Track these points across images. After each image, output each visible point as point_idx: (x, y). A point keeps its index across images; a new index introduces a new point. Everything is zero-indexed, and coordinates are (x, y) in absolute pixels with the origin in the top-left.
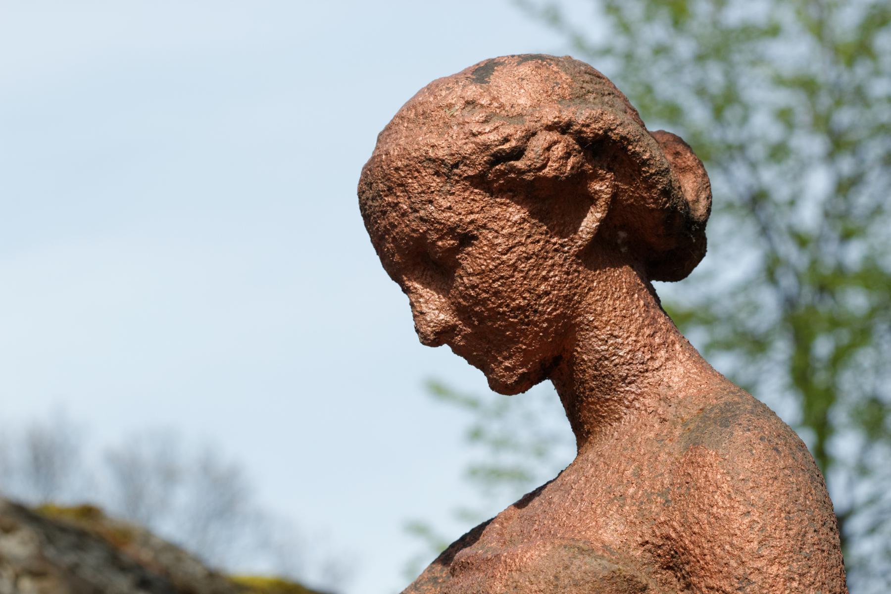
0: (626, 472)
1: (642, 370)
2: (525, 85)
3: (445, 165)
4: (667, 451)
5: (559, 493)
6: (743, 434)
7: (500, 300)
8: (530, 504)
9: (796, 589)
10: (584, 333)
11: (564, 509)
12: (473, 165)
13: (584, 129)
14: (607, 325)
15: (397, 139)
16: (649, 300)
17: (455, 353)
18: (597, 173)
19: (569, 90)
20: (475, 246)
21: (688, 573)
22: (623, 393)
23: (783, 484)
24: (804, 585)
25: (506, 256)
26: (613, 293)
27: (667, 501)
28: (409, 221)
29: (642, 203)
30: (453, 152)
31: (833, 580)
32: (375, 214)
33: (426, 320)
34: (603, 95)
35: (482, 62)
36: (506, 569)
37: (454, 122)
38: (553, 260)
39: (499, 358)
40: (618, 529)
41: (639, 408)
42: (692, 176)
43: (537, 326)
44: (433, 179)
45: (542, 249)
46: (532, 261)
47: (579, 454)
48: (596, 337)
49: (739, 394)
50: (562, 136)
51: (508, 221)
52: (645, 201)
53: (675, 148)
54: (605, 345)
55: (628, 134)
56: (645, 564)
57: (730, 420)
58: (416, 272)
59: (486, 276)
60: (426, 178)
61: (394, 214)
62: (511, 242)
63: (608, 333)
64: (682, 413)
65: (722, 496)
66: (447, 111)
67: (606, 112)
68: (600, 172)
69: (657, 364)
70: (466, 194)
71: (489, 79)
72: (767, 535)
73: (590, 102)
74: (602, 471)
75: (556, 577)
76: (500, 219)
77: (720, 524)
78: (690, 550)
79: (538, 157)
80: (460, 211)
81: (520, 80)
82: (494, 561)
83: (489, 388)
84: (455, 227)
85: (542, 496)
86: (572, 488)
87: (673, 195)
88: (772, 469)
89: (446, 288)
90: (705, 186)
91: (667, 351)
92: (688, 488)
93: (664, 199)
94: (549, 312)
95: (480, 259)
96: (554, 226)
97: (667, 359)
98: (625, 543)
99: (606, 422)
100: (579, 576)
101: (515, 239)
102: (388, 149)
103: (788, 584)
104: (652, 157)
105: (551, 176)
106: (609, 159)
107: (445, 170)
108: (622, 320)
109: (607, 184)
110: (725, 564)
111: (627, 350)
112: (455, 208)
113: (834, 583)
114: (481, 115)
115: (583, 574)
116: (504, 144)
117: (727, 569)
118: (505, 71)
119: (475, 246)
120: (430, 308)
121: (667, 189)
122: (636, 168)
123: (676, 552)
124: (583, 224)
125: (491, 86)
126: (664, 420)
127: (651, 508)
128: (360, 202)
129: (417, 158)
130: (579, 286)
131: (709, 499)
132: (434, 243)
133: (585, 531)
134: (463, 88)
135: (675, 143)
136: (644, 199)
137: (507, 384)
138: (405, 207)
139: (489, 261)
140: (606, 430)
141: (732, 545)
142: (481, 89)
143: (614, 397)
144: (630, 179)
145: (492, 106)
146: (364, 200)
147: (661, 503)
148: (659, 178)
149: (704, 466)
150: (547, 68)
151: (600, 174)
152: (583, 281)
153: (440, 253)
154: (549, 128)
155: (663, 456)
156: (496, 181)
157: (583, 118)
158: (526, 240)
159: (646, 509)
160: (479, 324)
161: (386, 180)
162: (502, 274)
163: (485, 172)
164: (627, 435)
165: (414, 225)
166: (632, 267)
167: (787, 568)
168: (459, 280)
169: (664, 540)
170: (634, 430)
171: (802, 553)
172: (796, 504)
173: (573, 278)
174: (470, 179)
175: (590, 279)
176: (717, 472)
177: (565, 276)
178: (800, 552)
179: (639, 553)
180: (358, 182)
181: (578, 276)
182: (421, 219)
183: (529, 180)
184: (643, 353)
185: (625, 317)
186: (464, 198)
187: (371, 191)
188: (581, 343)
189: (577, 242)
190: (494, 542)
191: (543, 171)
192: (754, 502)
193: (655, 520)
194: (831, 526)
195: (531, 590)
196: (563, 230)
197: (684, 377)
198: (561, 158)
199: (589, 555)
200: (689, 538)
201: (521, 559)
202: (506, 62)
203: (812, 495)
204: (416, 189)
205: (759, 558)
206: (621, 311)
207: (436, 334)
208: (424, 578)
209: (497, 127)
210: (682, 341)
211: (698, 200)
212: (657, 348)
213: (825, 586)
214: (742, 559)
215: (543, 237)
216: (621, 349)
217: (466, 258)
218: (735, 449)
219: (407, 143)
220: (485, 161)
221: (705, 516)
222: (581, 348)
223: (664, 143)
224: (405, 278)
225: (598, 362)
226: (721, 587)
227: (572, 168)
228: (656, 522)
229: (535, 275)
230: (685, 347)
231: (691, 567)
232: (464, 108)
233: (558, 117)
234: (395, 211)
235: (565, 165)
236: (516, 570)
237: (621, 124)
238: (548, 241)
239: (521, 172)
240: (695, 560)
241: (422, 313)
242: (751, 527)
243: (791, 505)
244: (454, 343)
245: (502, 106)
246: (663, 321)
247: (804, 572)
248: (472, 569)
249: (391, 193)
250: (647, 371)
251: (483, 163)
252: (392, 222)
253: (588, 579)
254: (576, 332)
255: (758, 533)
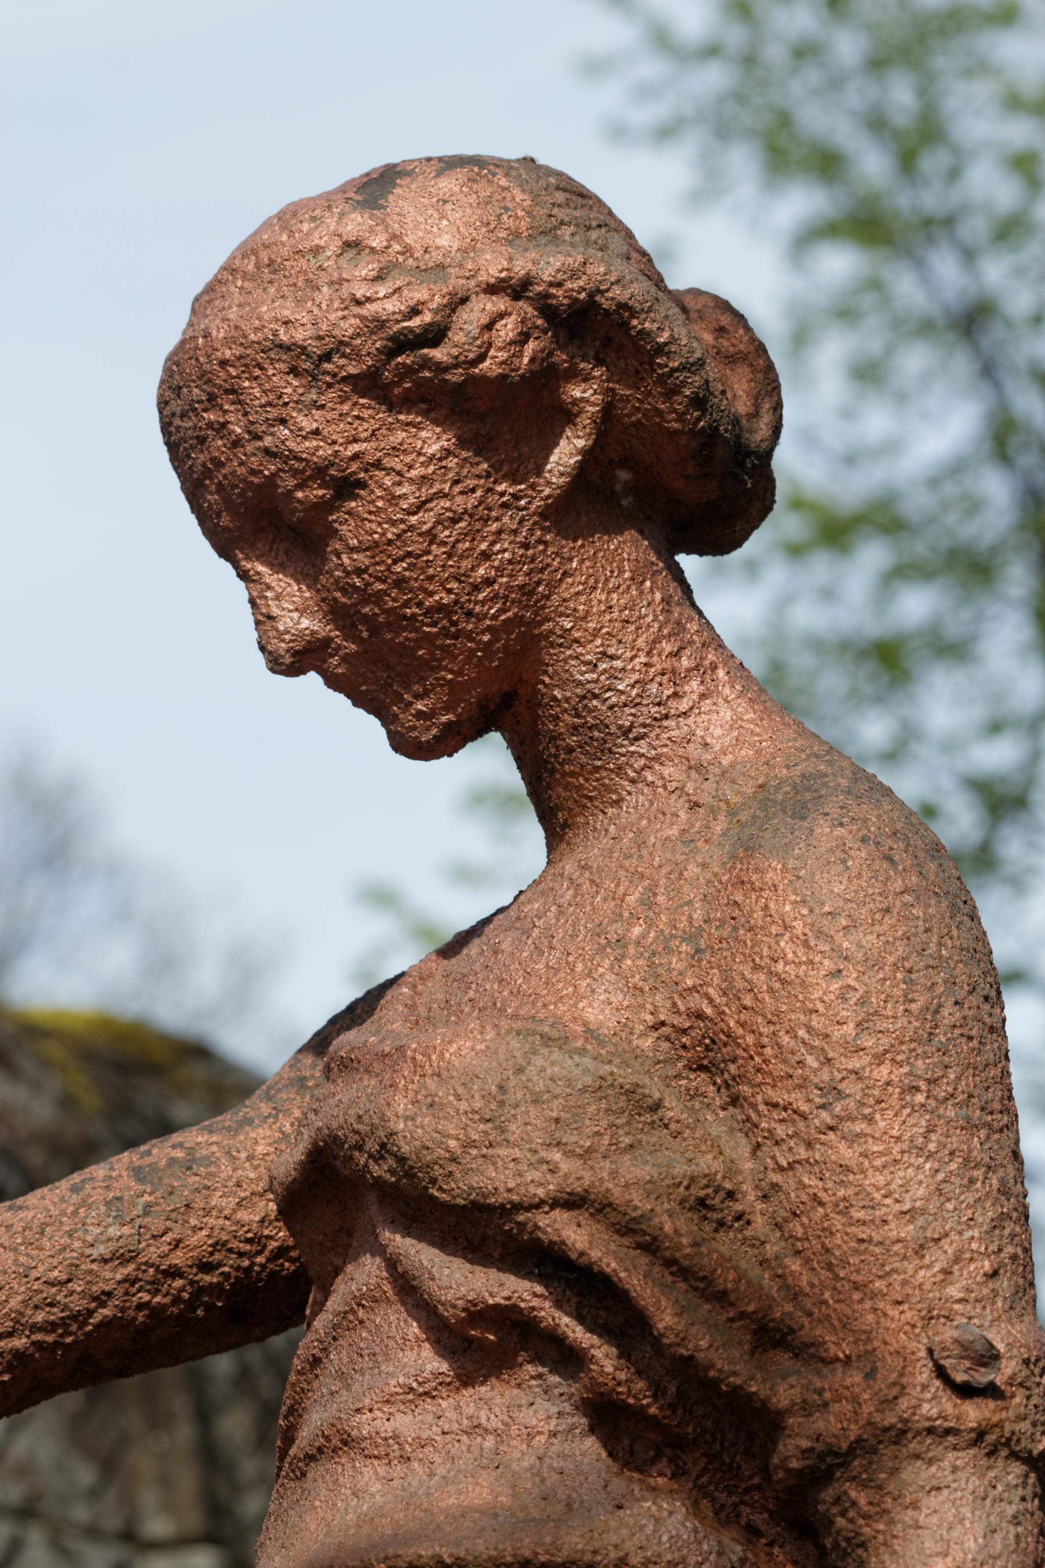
0: (628, 898)
1: (658, 715)
2: (449, 212)
3: (308, 355)
4: (700, 860)
5: (512, 934)
6: (832, 831)
7: (406, 594)
8: (465, 951)
9: (923, 1106)
10: (556, 651)
11: (520, 964)
12: (356, 355)
13: (553, 291)
14: (595, 636)
15: (224, 308)
16: (671, 591)
17: (329, 687)
18: (576, 368)
19: (528, 219)
20: (362, 498)
21: (734, 1079)
22: (624, 756)
23: (899, 921)
24: (936, 1099)
25: (416, 517)
26: (607, 580)
27: (698, 951)
28: (245, 455)
29: (657, 420)
30: (321, 333)
31: (987, 1088)
32: (186, 442)
33: (277, 630)
34: (589, 228)
35: (375, 170)
36: (415, 1072)
37: (323, 279)
38: (499, 524)
39: (406, 696)
40: (613, 999)
41: (653, 783)
42: (747, 370)
43: (472, 640)
44: (287, 381)
45: (480, 504)
46: (463, 524)
47: (549, 862)
48: (577, 658)
49: (828, 758)
50: (513, 302)
51: (419, 454)
52: (662, 417)
53: (718, 320)
54: (593, 671)
55: (630, 299)
56: (659, 1062)
57: (810, 805)
58: (260, 545)
59: (381, 552)
60: (275, 379)
61: (220, 443)
62: (424, 493)
63: (598, 650)
64: (728, 792)
65: (793, 942)
66: (311, 259)
67: (591, 260)
68: (582, 365)
69: (684, 705)
70: (346, 408)
71: (387, 201)
72: (871, 1011)
73: (564, 241)
74: (587, 896)
75: (501, 1088)
76: (405, 450)
77: (789, 992)
78: (737, 1038)
79: (471, 341)
80: (333, 437)
81: (441, 203)
82: (395, 1057)
83: (390, 748)
84: (327, 466)
85: (484, 938)
86: (535, 926)
87: (711, 407)
88: (880, 894)
89: (311, 572)
90: (769, 389)
91: (702, 682)
92: (735, 929)
93: (695, 414)
94: (493, 615)
95: (371, 521)
96: (501, 463)
97: (703, 696)
98: (625, 1025)
99: (596, 807)
100: (541, 1084)
101: (431, 487)
102: (207, 328)
103: (908, 1098)
104: (673, 341)
105: (495, 374)
106: (598, 343)
107: (307, 365)
108: (623, 627)
109: (595, 387)
110: (798, 1063)
111: (632, 681)
112: (325, 432)
113: (990, 1095)
114: (370, 267)
115: (548, 1082)
116: (410, 319)
117: (800, 1071)
118: (414, 186)
119: (362, 498)
120: (284, 609)
121: (701, 395)
122: (646, 359)
123: (713, 1042)
124: (553, 458)
125: (388, 214)
126: (697, 805)
127: (671, 963)
128: (161, 419)
129: (258, 343)
130: (545, 569)
131: (770, 947)
132: (289, 493)
133: (555, 1004)
134: (340, 218)
135: (718, 312)
136: (660, 413)
137: (420, 742)
138: (239, 431)
139: (386, 526)
140: (595, 822)
141: (809, 1029)
142: (371, 219)
143: (608, 763)
144: (635, 379)
145: (390, 250)
146: (167, 416)
147: (687, 953)
148: (686, 377)
149: (762, 889)
150: (489, 181)
151: (583, 369)
152: (554, 560)
153: (300, 511)
154: (492, 289)
155: (693, 870)
156: (398, 384)
157: (551, 270)
158: (451, 488)
159: (661, 964)
160: (370, 636)
161: (205, 383)
162: (409, 549)
163: (378, 369)
164: (631, 830)
165: (254, 462)
166: (641, 532)
167: (906, 1069)
168: (335, 559)
169: (693, 1019)
170: (644, 822)
171: (933, 1043)
172: (923, 955)
173: (534, 555)
174: (353, 381)
175: (566, 556)
176: (785, 900)
177: (521, 552)
178: (930, 1041)
179: (648, 1042)
180: (156, 384)
181: (544, 551)
182: (267, 451)
183: (455, 383)
184: (661, 685)
185: (627, 622)
186: (341, 415)
187: (179, 402)
188: (550, 670)
189: (542, 491)
190: (397, 1021)
191: (481, 366)
192: (849, 954)
193: (676, 984)
194: (985, 992)
195: (458, 1110)
196: (517, 470)
197: (731, 727)
198: (512, 343)
199: (560, 1048)
200: (736, 1017)
201: (441, 1055)
202: (417, 170)
203: (951, 938)
204: (258, 399)
205: (856, 1051)
206: (620, 611)
207: (296, 654)
208: (283, 1078)
209: (399, 288)
210: (730, 664)
211: (758, 412)
212: (685, 677)
213: (973, 1100)
214: (827, 1054)
215: (482, 481)
216: (620, 679)
217: (347, 520)
218: (817, 859)
219: (241, 317)
220: (377, 349)
221: (763, 977)
222: (551, 678)
223: (699, 310)
224: (241, 556)
225: (580, 702)
226: (791, 1104)
227: (532, 360)
228: (679, 988)
229: (467, 549)
230: (735, 673)
231: (739, 1068)
232: (341, 254)
233: (507, 270)
234: (222, 438)
235: (520, 355)
236: (433, 1075)
237: (618, 282)
238: (490, 490)
239: (441, 368)
240: (745, 1055)
241: (270, 617)
242: (842, 997)
243: (914, 957)
244: (327, 670)
245: (407, 251)
246: (695, 628)
247: (936, 1075)
248: (357, 1070)
249: (214, 406)
250: (666, 717)
251: (375, 352)
252: (216, 457)
253: (558, 1091)
254: (542, 649)
255: (855, 1008)
